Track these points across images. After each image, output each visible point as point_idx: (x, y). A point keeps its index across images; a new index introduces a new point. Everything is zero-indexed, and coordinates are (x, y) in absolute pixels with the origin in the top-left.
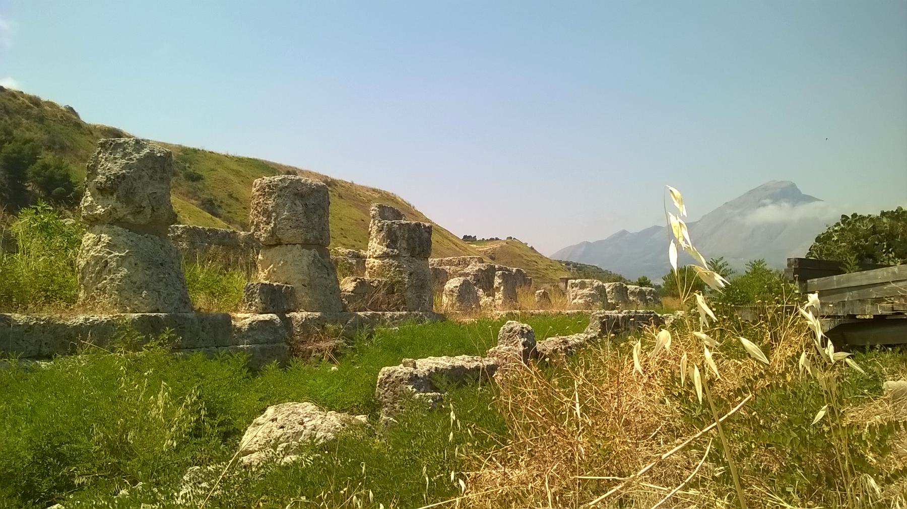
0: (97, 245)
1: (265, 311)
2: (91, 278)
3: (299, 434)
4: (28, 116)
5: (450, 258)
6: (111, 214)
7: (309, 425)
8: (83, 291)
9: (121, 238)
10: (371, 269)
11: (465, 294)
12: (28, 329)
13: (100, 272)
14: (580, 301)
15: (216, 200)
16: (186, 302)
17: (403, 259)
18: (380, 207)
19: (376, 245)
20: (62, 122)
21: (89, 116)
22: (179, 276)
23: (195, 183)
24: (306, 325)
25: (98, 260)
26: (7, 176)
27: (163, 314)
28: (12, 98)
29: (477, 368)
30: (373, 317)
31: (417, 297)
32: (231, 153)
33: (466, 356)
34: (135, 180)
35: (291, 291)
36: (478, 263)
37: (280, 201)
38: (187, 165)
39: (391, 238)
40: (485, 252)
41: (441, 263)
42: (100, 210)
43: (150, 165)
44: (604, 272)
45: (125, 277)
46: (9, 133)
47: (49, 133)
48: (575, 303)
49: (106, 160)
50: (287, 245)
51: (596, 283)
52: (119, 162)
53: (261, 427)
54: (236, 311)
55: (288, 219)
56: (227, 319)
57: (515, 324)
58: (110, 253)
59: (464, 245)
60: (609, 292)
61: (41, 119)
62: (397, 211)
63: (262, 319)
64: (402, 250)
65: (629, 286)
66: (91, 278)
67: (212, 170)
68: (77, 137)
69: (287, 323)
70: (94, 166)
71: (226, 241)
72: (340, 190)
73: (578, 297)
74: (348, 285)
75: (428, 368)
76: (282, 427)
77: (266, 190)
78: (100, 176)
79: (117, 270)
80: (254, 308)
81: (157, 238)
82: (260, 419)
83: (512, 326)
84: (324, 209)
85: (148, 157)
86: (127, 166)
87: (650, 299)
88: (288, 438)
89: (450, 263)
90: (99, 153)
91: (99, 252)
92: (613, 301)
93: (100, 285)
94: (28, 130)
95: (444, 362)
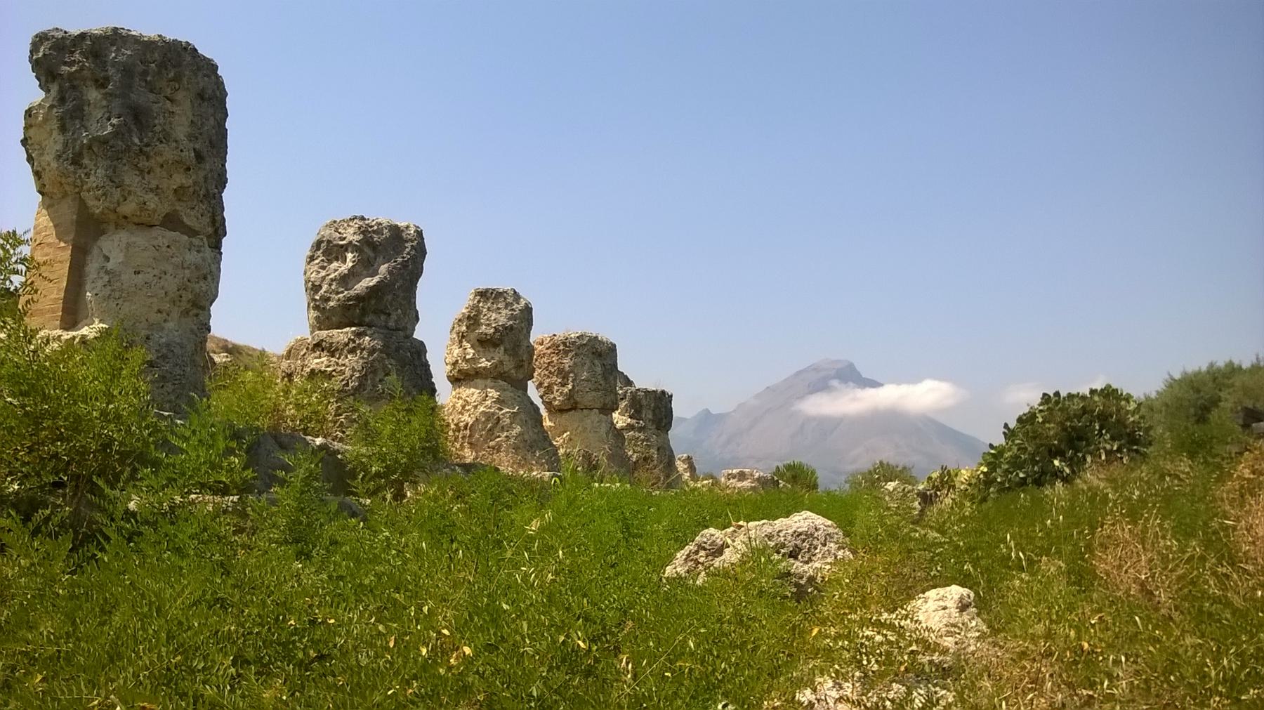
2: (481, 436)
6: (496, 367)
25: (488, 416)
49: (489, 309)
78: (484, 327)
79: (510, 428)
86: (512, 317)
91: (490, 408)
93: (492, 443)
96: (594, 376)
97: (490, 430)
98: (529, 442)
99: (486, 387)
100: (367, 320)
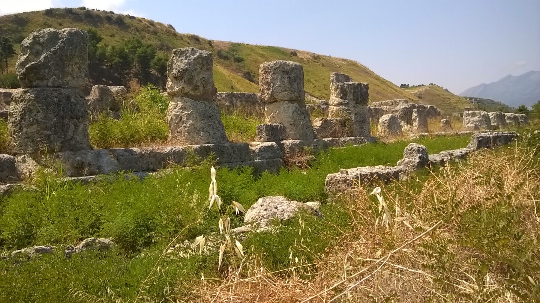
0: (176, 108)
1: (269, 140)
2: (174, 126)
3: (275, 214)
4: (149, 32)
5: (387, 101)
6: (181, 91)
7: (280, 209)
8: (170, 133)
9: (188, 104)
10: (332, 112)
11: (393, 124)
12: (142, 155)
13: (178, 123)
14: (472, 125)
15: (252, 72)
16: (224, 137)
17: (351, 106)
18: (336, 74)
19: (334, 98)
20: (166, 33)
21: (180, 30)
22: (220, 123)
23: (239, 63)
24: (291, 147)
25: (177, 116)
26: (140, 66)
27: (212, 145)
28: (140, 23)
29: (388, 173)
30: (332, 141)
31: (360, 128)
32: (259, 44)
33: (382, 166)
34: (193, 71)
35: (283, 128)
36: (404, 104)
37: (275, 76)
38: (235, 53)
39: (343, 93)
40: (415, 94)
41: (381, 105)
42: (176, 89)
43: (200, 62)
44: (495, 103)
45: (191, 125)
46: (139, 42)
47: (160, 40)
48: (468, 126)
50: (280, 101)
51: (483, 113)
52: (184, 61)
53: (255, 209)
54: (254, 141)
55: (279, 86)
56: (247, 146)
57: (414, 145)
58: (183, 112)
59: (401, 90)
60: (492, 118)
61: (155, 33)
62: (347, 76)
63: (267, 145)
64: (350, 100)
65: (506, 114)
66: (174, 126)
67: (249, 55)
68: (175, 42)
69: (281, 146)
70: (171, 65)
71: (250, 99)
72: (323, 61)
73: (470, 123)
74: (317, 123)
75: (355, 174)
76: (266, 210)
77: (267, 70)
79: (187, 122)
80: (262, 139)
81: (207, 102)
82: (255, 205)
83: (412, 146)
84: (300, 79)
85: (199, 57)
86: (188, 63)
87: (522, 122)
88: (269, 216)
89: (386, 104)
90: (173, 57)
92: (495, 124)
93: (179, 130)
94: (149, 39)
95: (366, 170)
96: (284, 84)
97: (177, 123)
98: (198, 128)
99: (178, 101)
100: (34, 84)
